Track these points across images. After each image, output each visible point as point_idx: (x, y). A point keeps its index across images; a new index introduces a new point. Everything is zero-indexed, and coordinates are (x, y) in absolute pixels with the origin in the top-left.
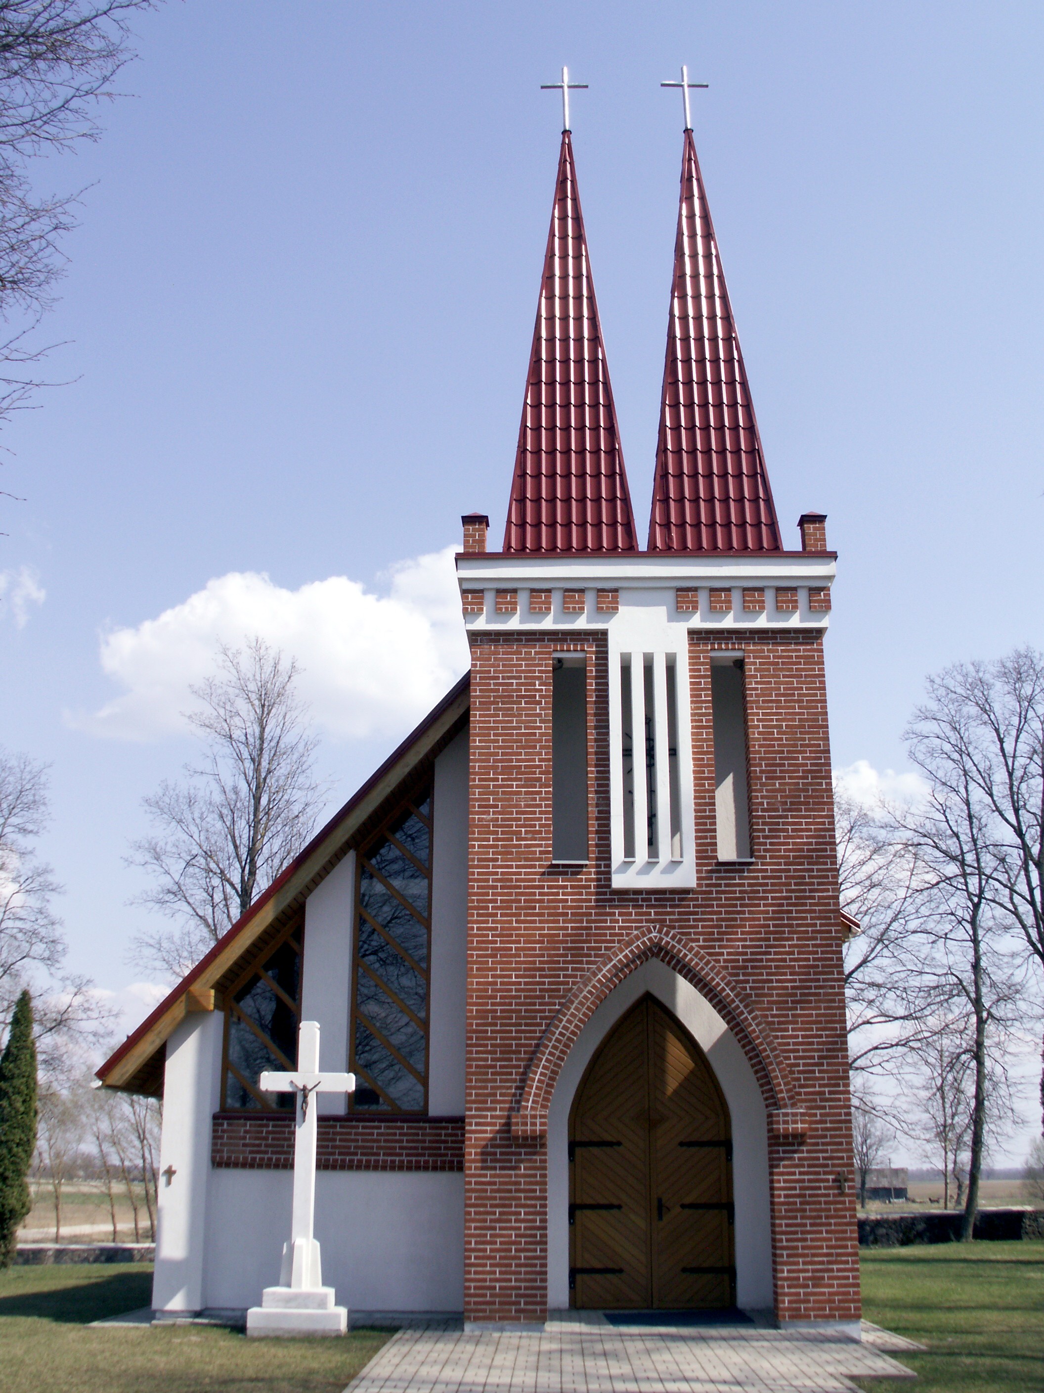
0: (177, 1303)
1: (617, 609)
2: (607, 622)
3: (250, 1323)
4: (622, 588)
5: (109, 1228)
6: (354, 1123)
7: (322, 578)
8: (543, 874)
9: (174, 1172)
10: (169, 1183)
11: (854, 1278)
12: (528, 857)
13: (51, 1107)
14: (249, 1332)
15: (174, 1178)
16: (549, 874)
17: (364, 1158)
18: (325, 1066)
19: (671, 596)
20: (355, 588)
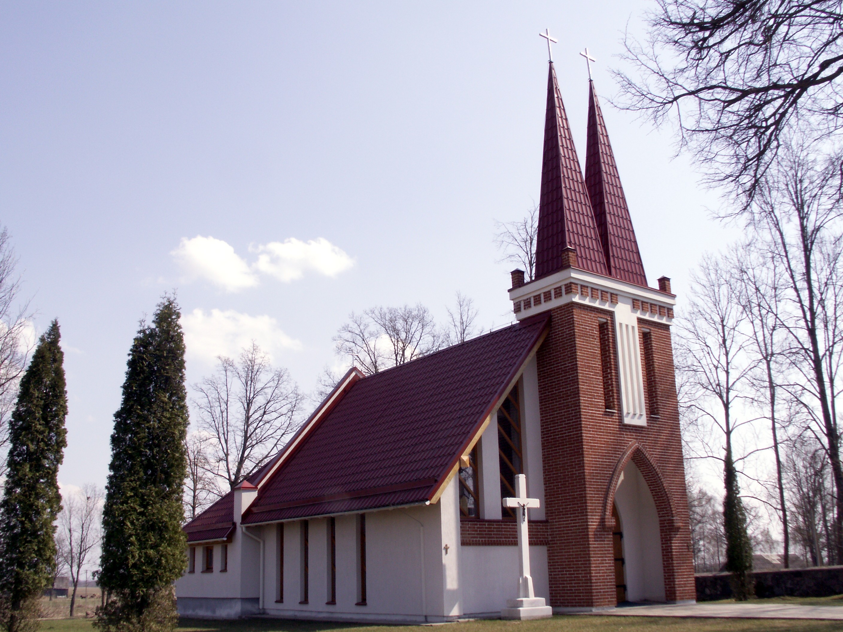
0: (455, 612)
1: (617, 303)
2: (614, 308)
3: (522, 615)
4: (619, 295)
5: (88, 588)
6: (508, 523)
7: (220, 239)
8: (603, 414)
9: (449, 548)
10: (446, 553)
11: (551, 575)
12: (596, 406)
13: (137, 523)
14: (522, 619)
15: (448, 550)
16: (605, 415)
17: (481, 539)
18: (528, 496)
19: (630, 301)
20: (231, 249)
